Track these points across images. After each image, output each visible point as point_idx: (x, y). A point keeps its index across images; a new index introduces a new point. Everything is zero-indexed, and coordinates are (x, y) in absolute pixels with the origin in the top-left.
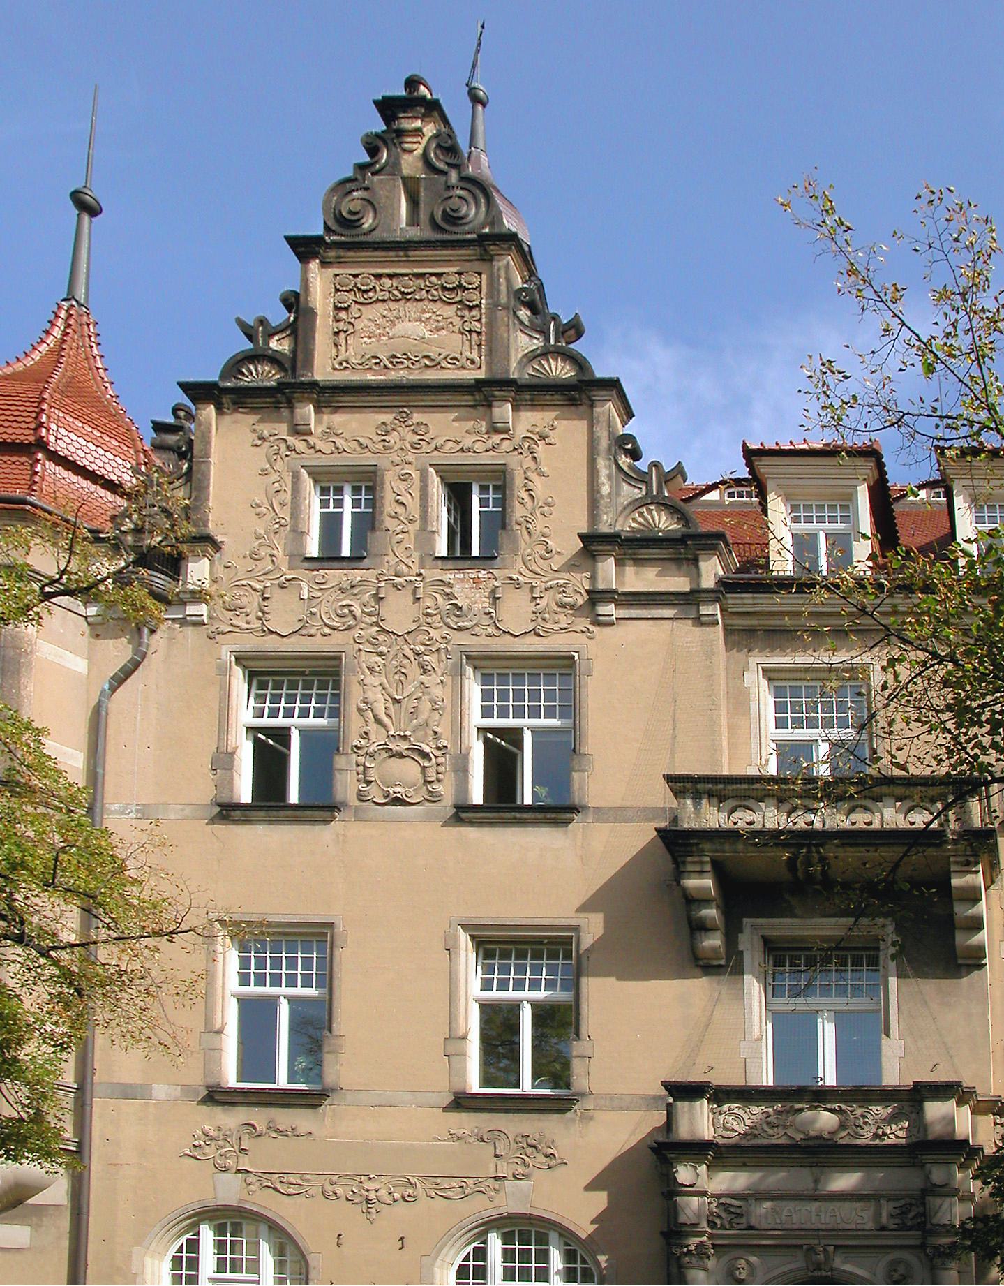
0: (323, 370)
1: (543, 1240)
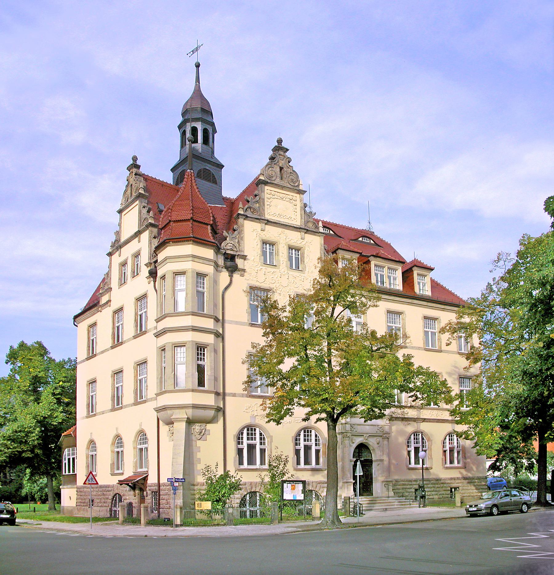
0: (267, 217)
1: (255, 430)
